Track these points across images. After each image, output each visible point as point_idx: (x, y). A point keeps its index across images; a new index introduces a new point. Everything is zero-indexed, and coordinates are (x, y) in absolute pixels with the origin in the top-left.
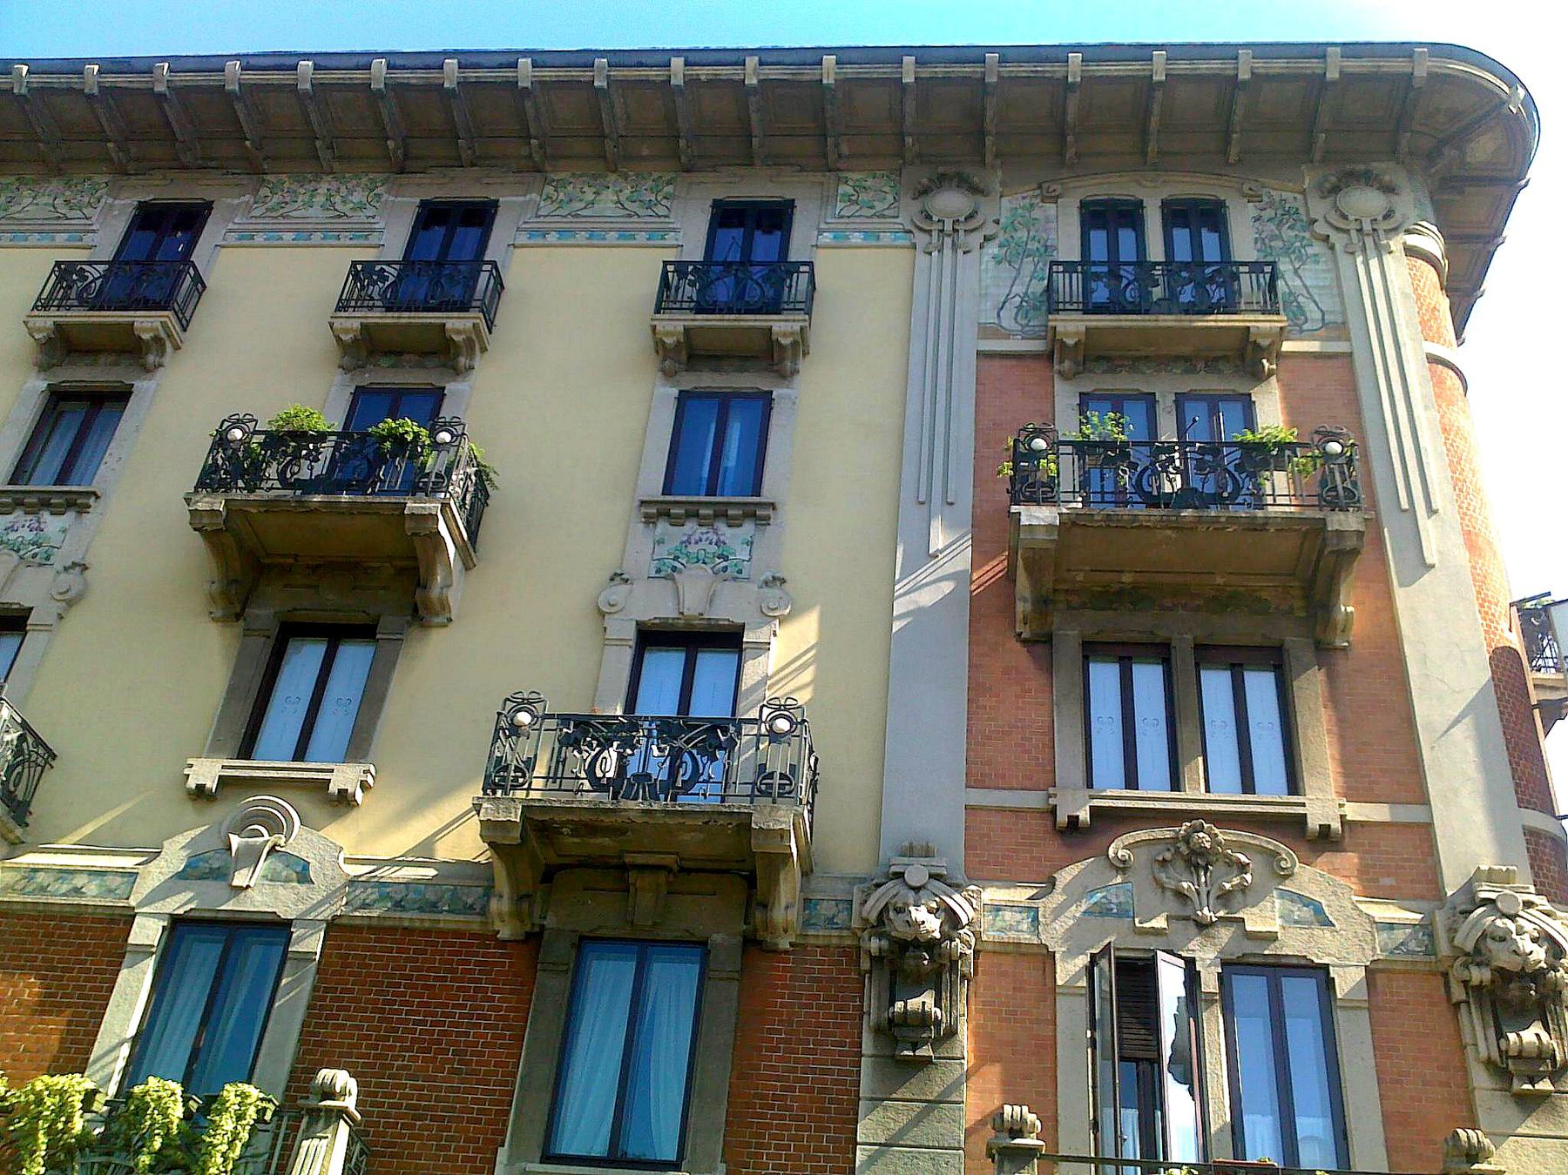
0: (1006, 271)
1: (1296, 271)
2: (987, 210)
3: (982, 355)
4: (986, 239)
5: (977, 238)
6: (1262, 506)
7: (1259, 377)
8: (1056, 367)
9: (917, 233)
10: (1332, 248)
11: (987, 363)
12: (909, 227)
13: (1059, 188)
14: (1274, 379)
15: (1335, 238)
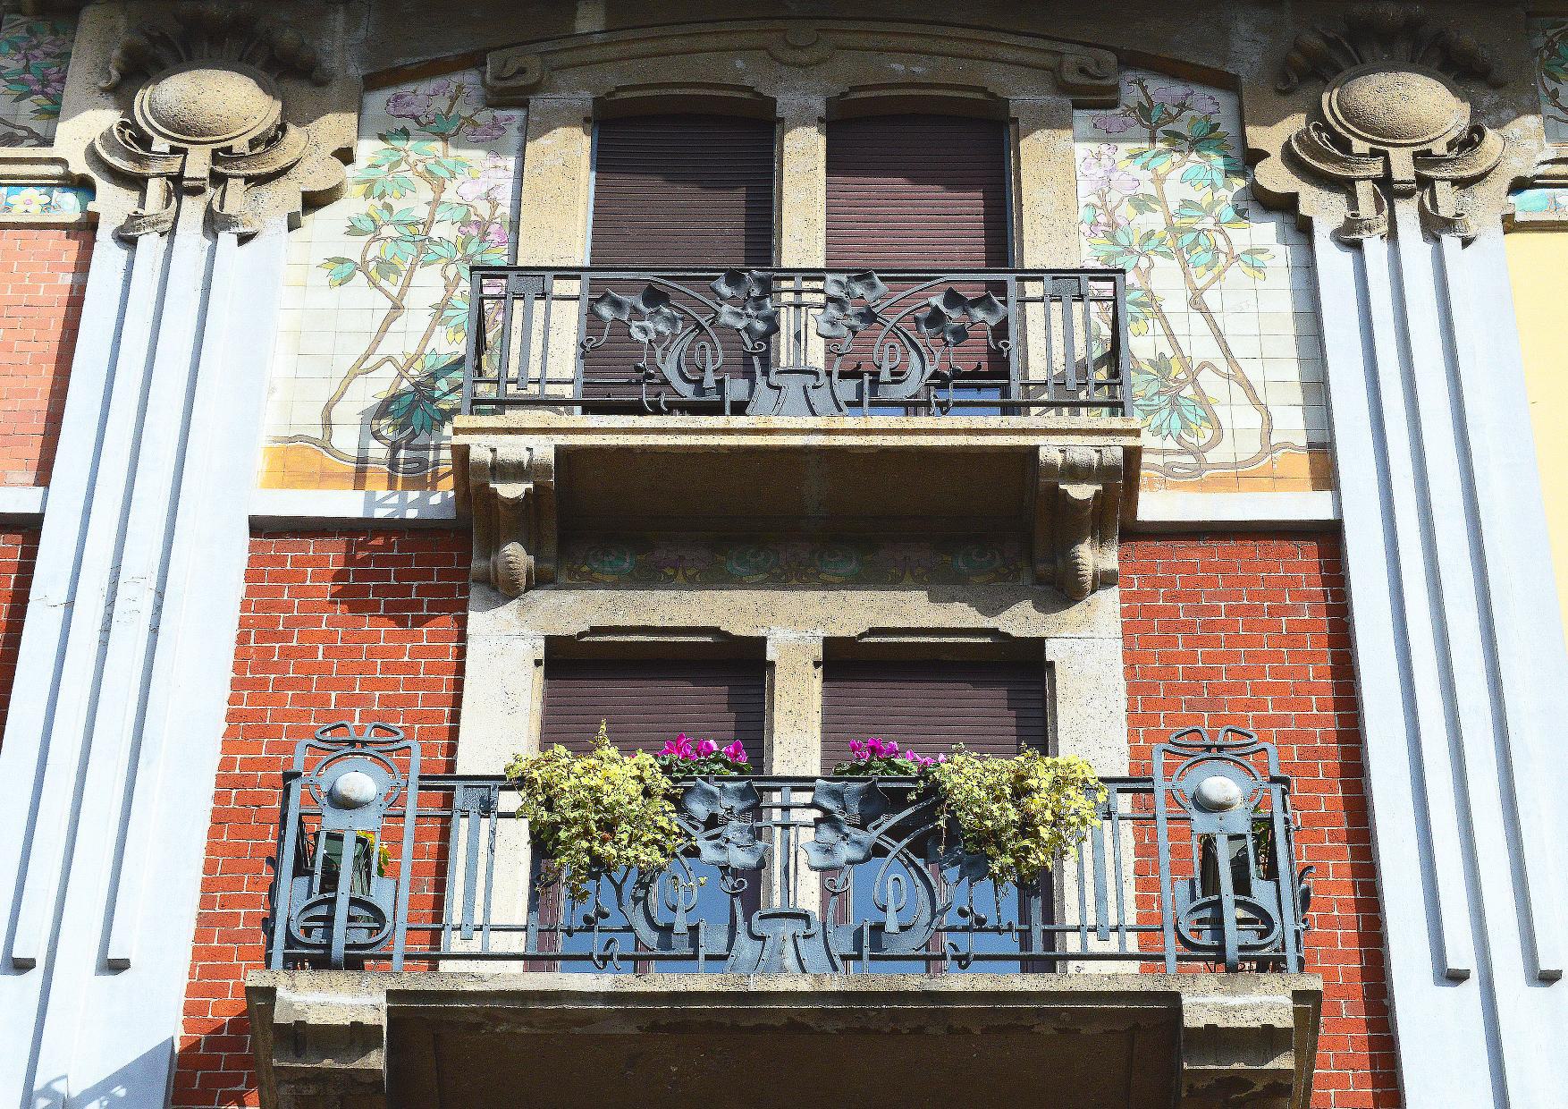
0: (364, 301)
1: (1196, 302)
2: (313, 145)
3: (261, 528)
4: (313, 201)
5: (286, 195)
6: (1047, 963)
7: (1063, 589)
8: (477, 565)
9: (103, 185)
10: (1304, 228)
11: (273, 546)
12: (79, 166)
13: (534, 64)
14: (1108, 603)
15: (1326, 211)
